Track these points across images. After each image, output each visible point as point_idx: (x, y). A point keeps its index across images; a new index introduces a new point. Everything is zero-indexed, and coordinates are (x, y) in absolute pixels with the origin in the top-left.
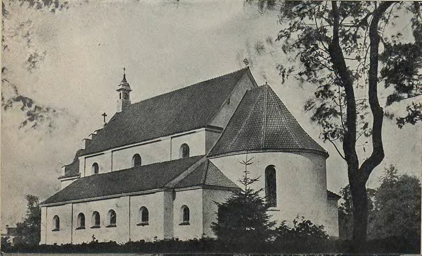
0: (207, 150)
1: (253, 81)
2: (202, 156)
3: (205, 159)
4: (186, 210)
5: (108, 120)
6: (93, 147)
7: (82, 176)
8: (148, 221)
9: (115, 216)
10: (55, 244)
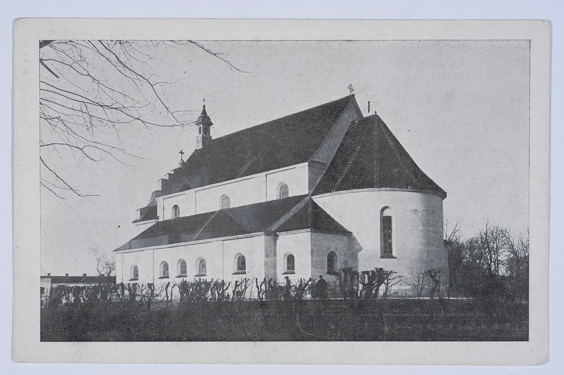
0: (310, 189)
1: (358, 111)
2: (306, 196)
3: (308, 198)
4: (291, 259)
5: (186, 159)
6: (178, 181)
7: (161, 220)
8: (245, 269)
9: (167, 269)
10: (85, 275)
